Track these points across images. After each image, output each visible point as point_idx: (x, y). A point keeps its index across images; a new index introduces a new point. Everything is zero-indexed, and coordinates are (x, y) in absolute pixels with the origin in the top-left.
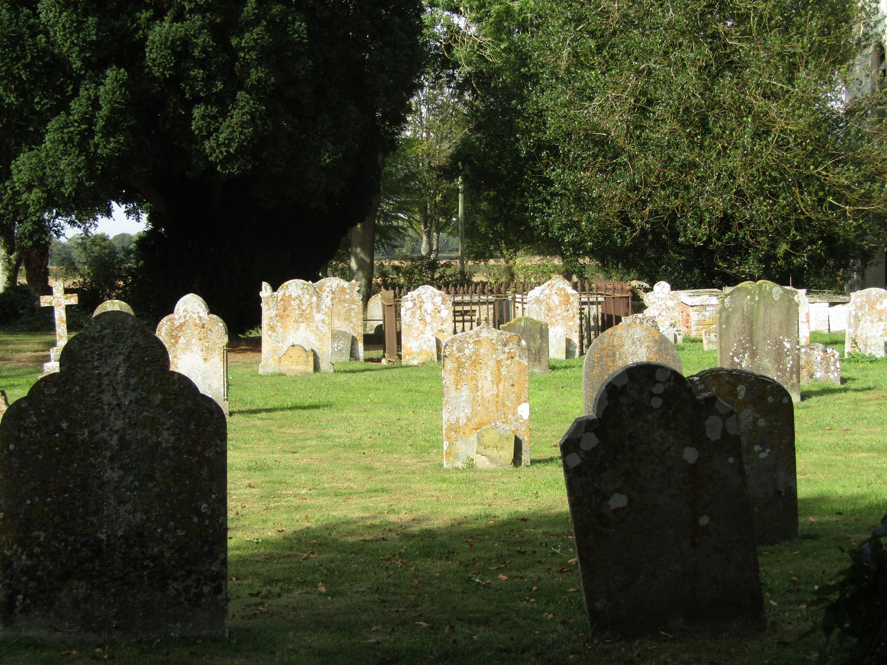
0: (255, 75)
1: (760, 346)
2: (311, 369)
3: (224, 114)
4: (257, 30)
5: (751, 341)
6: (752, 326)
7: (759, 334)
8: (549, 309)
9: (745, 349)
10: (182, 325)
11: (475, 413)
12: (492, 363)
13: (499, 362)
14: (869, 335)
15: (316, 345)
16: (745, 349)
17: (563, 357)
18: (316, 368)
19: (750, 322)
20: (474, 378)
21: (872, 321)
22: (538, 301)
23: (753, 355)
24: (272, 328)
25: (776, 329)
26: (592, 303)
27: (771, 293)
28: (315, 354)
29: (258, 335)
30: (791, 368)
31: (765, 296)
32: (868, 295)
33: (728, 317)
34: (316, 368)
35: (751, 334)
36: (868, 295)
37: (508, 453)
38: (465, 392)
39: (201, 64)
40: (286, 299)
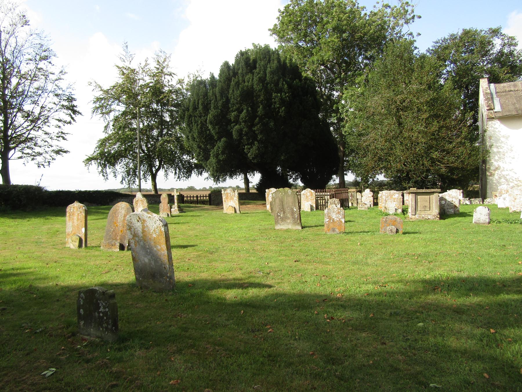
0: (259, 137)
1: (286, 210)
2: (234, 212)
3: (252, 147)
4: (259, 125)
5: (283, 208)
6: (283, 203)
7: (285, 206)
8: (307, 197)
9: (281, 211)
10: (138, 200)
11: (73, 231)
12: (77, 214)
13: (78, 214)
14: (390, 206)
15: (234, 205)
16: (281, 211)
17: (309, 210)
18: (235, 212)
19: (282, 202)
20: (73, 219)
21: (391, 202)
22: (304, 194)
23: (284, 213)
24: (225, 201)
25: (291, 204)
26: (326, 195)
27: (288, 192)
28: (235, 208)
29: (179, 204)
30: (297, 217)
31: (286, 193)
32: (390, 193)
33: (275, 200)
34: (235, 212)
35: (283, 205)
36: (390, 193)
37: (77, 244)
38: (71, 223)
39: (245, 135)
40: (227, 194)
